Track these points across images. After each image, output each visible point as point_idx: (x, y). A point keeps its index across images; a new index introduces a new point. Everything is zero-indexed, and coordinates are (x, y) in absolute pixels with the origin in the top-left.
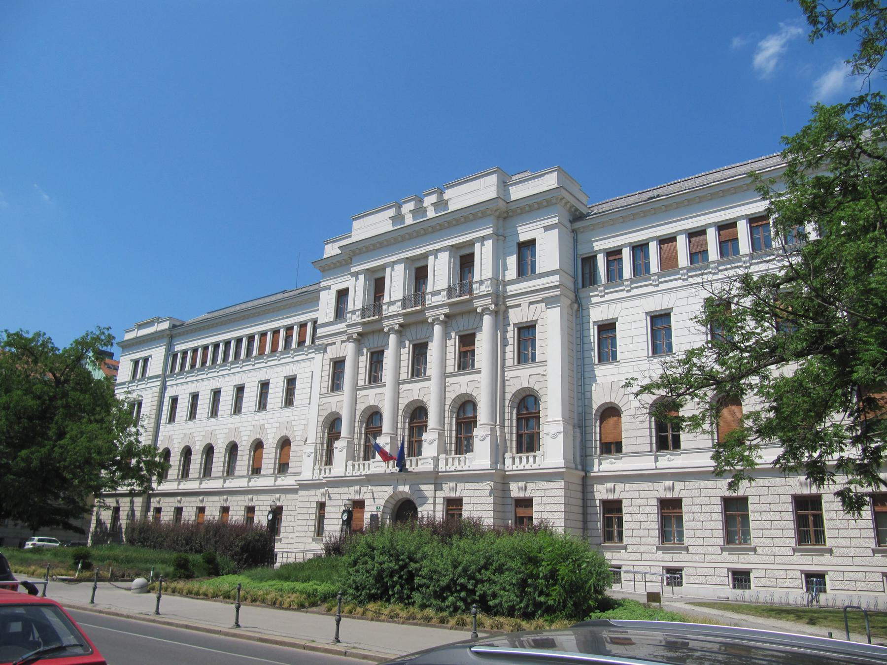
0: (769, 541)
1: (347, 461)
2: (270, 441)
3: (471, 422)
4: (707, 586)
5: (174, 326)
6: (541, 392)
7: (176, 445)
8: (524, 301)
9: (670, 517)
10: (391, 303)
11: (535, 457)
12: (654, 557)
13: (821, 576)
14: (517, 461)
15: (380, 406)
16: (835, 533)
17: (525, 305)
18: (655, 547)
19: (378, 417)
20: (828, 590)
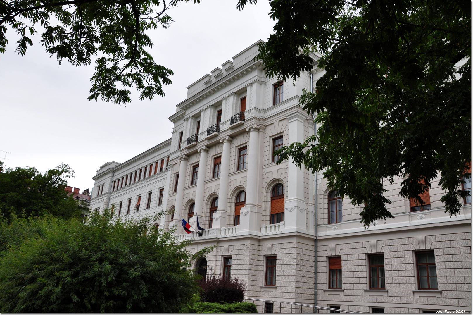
0: (453, 287)
3: (274, 197)
6: (284, 181)
8: (275, 120)
10: (225, 123)
11: (279, 225)
12: (411, 300)
14: (269, 229)
15: (244, 186)
17: (276, 123)
18: (411, 292)
19: (281, 187)
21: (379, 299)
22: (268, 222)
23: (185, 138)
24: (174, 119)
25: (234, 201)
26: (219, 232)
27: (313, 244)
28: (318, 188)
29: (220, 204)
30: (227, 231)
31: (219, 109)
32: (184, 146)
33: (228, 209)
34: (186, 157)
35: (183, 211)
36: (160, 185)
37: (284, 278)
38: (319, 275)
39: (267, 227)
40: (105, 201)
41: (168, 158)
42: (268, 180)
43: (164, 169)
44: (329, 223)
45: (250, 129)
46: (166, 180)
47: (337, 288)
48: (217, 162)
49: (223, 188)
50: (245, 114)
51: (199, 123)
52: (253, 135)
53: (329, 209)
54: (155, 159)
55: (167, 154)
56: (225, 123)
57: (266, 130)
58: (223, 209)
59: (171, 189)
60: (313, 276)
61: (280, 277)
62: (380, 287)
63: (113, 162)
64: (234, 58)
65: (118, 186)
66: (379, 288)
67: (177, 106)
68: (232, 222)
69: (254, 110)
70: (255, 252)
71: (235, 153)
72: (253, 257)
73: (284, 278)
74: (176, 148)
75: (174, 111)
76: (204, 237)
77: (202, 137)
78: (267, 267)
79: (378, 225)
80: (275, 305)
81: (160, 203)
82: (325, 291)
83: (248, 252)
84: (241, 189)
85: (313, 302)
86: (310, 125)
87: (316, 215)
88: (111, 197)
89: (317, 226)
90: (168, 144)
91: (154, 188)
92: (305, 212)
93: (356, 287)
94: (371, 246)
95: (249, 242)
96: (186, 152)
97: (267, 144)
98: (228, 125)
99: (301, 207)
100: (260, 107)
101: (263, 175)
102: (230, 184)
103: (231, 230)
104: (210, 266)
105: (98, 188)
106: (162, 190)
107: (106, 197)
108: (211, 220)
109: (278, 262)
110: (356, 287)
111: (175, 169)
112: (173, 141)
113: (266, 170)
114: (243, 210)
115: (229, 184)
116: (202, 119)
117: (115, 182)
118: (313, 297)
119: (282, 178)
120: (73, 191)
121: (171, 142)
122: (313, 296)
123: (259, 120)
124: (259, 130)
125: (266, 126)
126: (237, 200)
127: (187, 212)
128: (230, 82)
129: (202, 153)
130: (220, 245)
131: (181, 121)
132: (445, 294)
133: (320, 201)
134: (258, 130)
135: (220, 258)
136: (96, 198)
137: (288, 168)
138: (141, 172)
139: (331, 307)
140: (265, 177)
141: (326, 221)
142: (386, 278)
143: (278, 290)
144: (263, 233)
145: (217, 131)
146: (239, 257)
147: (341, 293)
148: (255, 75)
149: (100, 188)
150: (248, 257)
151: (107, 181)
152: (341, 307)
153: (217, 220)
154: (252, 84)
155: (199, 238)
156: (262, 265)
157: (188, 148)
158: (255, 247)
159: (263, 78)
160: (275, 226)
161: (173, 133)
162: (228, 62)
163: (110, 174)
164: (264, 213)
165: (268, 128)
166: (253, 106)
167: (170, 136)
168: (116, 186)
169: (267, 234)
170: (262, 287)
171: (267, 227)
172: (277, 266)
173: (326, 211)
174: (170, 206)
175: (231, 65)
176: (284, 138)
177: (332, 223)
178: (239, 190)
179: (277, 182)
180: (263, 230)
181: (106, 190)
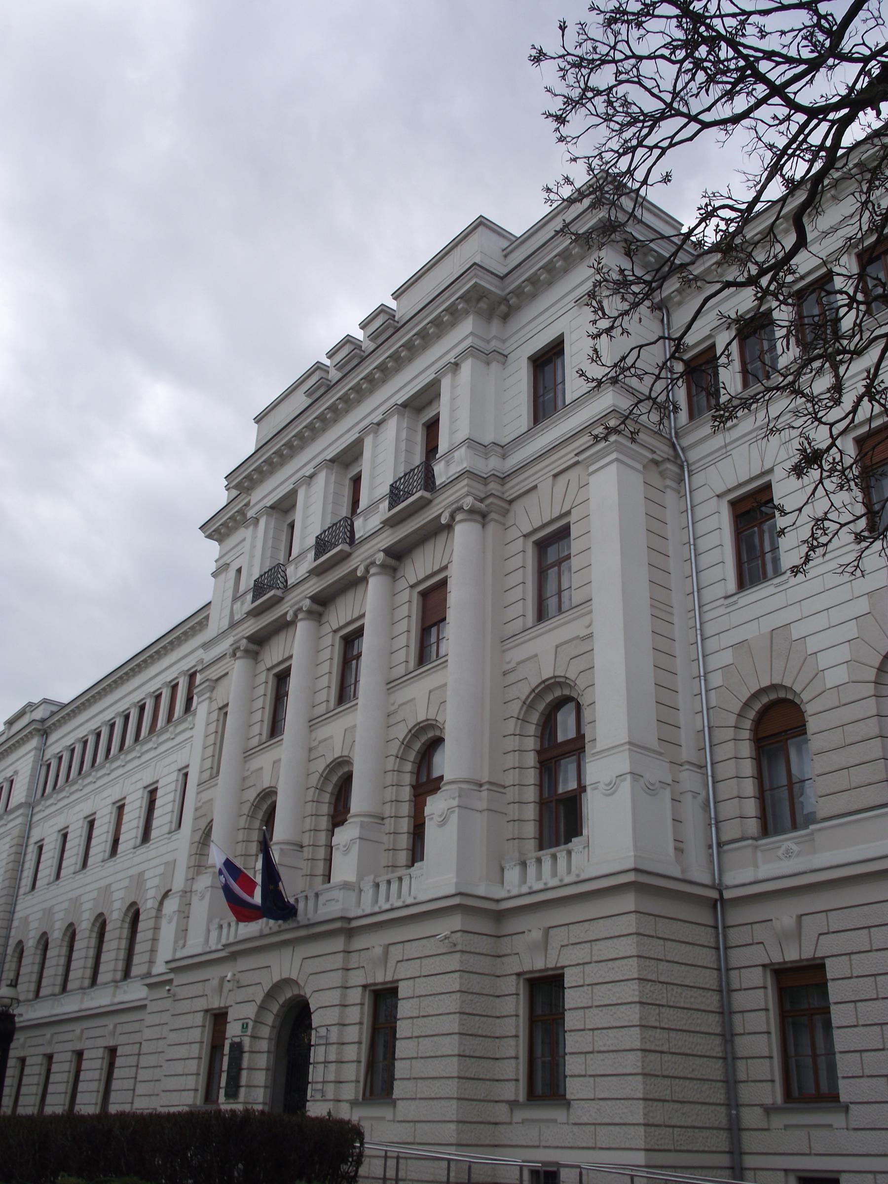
6: (581, 683)
8: (541, 474)
11: (569, 853)
14: (532, 870)
22: (531, 845)
24: (219, 528)
25: (407, 779)
26: (353, 896)
28: (713, 703)
29: (360, 800)
30: (383, 887)
31: (353, 472)
33: (388, 810)
34: (252, 647)
38: (745, 1045)
39: (524, 864)
40: (16, 832)
42: (524, 691)
44: (766, 831)
45: (452, 517)
49: (363, 735)
52: (464, 533)
53: (759, 777)
56: (373, 506)
60: (717, 1051)
61: (580, 1059)
63: (45, 701)
64: (396, 296)
68: (403, 857)
69: (463, 450)
70: (484, 964)
73: (597, 1064)
75: (218, 496)
78: (533, 1021)
82: (769, 1110)
83: (454, 962)
84: (431, 734)
86: (669, 482)
88: (35, 819)
92: (667, 794)
95: (456, 922)
97: (517, 561)
100: (487, 439)
101: (505, 674)
102: (392, 720)
103: (394, 886)
104: (323, 1031)
107: (19, 820)
109: (571, 998)
113: (516, 655)
114: (435, 806)
117: (49, 766)
118: (720, 1141)
119: (571, 675)
122: (724, 1135)
123: (485, 480)
124: (484, 516)
125: (511, 502)
126: (418, 773)
128: (385, 372)
130: (359, 943)
134: (481, 516)
135: (355, 996)
137: (590, 636)
140: (511, 678)
141: (753, 826)
143: (581, 1112)
144: (513, 885)
146: (422, 986)
147: (837, 1120)
150: (454, 983)
156: (513, 1008)
158: (484, 945)
162: (382, 310)
163: (34, 742)
164: (513, 811)
166: (462, 434)
170: (513, 1104)
172: (568, 1016)
173: (749, 787)
176: (574, 531)
177: (777, 833)
178: (423, 739)
180: (512, 875)
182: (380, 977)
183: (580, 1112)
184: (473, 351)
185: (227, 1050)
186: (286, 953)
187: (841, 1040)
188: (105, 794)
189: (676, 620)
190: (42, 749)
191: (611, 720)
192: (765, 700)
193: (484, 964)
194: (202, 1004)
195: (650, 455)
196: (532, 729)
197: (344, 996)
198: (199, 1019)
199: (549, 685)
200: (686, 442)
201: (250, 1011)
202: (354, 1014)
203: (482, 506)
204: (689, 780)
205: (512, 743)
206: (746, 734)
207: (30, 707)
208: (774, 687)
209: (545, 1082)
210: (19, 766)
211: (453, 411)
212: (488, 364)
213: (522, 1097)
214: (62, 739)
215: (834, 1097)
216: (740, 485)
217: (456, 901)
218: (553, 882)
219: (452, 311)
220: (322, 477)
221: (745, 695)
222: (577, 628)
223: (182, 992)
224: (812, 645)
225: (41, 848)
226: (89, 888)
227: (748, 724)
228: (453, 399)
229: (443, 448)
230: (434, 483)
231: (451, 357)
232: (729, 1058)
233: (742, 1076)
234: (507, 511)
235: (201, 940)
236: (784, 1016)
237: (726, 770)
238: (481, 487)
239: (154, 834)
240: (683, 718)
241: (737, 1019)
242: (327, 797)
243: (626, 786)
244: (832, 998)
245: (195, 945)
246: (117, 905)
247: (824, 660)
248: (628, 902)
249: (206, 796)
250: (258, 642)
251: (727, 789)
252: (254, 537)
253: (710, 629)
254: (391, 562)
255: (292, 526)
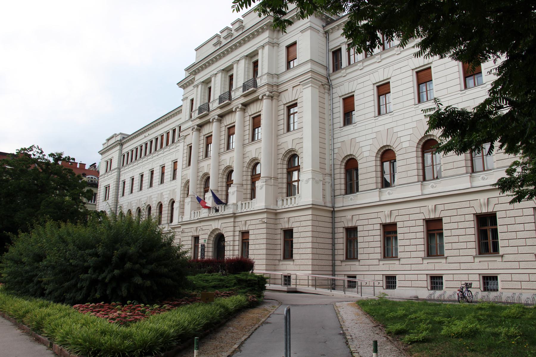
1: (191, 211)
2: (166, 203)
4: (412, 288)
5: (124, 138)
7: (166, 199)
9: (434, 234)
10: (237, 89)
11: (295, 198)
12: (376, 268)
13: (494, 278)
16: (505, 243)
18: (421, 259)
20: (444, 288)
21: (437, 266)
22: (285, 195)
23: (196, 106)
24: (184, 85)
27: (330, 215)
30: (244, 205)
31: (230, 74)
32: (196, 115)
33: (244, 182)
35: (198, 186)
36: (173, 158)
37: (301, 251)
41: (180, 127)
42: (283, 151)
43: (176, 140)
44: (346, 193)
46: (177, 152)
47: (392, 257)
48: (231, 132)
50: (257, 81)
51: (210, 88)
54: (166, 129)
55: (178, 123)
56: (237, 89)
57: (280, 97)
58: (238, 183)
59: (185, 162)
62: (492, 252)
63: (121, 134)
65: (136, 156)
66: (491, 253)
67: (187, 70)
68: (249, 196)
69: (266, 76)
70: (272, 226)
71: (249, 123)
72: (270, 231)
73: (301, 251)
74: (188, 117)
75: (182, 75)
76: (220, 213)
77: (214, 105)
78: (285, 241)
79: (431, 188)
80: (293, 277)
81: (174, 178)
82: (342, 261)
83: (264, 226)
84: (256, 161)
85: (331, 273)
86: (326, 91)
87: (333, 186)
88: (121, 173)
89: (334, 196)
90: (179, 111)
91: (156, 166)
92: (321, 183)
93: (371, 256)
94: (386, 216)
95: (265, 216)
96: (199, 122)
98: (240, 92)
99: (316, 178)
100: (274, 72)
101: (278, 146)
104: (228, 242)
105: (105, 164)
106: (175, 163)
108: (227, 195)
110: (371, 256)
111: (189, 140)
112: (183, 108)
115: (219, 164)
116: (212, 84)
117: (124, 155)
119: (297, 149)
120: (78, 166)
121: (181, 110)
123: (272, 86)
124: (272, 97)
125: (280, 93)
127: (203, 186)
128: (241, 44)
129: (264, 101)
130: (237, 220)
131: (191, 88)
132: (506, 258)
133: (337, 171)
134: (271, 97)
135: (237, 233)
136: (104, 174)
137: (302, 138)
138: (128, 155)
139: (348, 277)
141: (343, 192)
142: (444, 244)
145: (254, 87)
148: (265, 36)
149: (109, 163)
151: (115, 154)
152: (357, 276)
153: (233, 194)
154: (263, 47)
155: (216, 214)
156: (280, 238)
157: (200, 118)
158: (272, 221)
159: (275, 40)
160: (291, 199)
161: (183, 100)
163: (118, 148)
165: (283, 95)
167: (181, 103)
168: (127, 159)
169: (283, 207)
171: (283, 200)
174: (185, 181)
175: (241, 24)
179: (293, 153)
180: (280, 203)
181: (115, 165)
182: (244, 229)
183: (296, 262)
184: (269, 43)
185: (200, 246)
186: (217, 222)
187: (360, 245)
188: (146, 167)
189: (326, 133)
190: (121, 150)
191: (306, 162)
192: (348, 158)
193: (272, 226)
194: (191, 234)
195: (321, 84)
196: (285, 162)
197: (234, 234)
198: (190, 238)
199: (290, 151)
200: (332, 78)
201: (207, 237)
202: (237, 238)
203: (271, 94)
204: (328, 179)
205: (280, 166)
206: (343, 167)
207: (115, 135)
208: (351, 155)
209: (288, 254)
210: (113, 155)
211: (262, 58)
212: (273, 47)
213: (282, 258)
214: (128, 147)
215: (357, 259)
216: (346, 95)
217: (265, 210)
218: (291, 206)
219: (262, 28)
220: (219, 75)
221: (343, 157)
222: (298, 135)
223: (186, 230)
224: (361, 144)
225: (124, 183)
226: (143, 197)
227: (344, 164)
228: (262, 65)
229: (259, 74)
230: (257, 84)
231: (262, 44)
232: (333, 249)
233: (336, 253)
234: (279, 96)
235: (189, 216)
236: (347, 239)
237: (337, 176)
238: (271, 88)
239: (125, 194)
240: (327, 162)
241: (336, 240)
242: (225, 177)
243: (311, 181)
244: (358, 236)
245: (186, 218)
246: (154, 202)
247: (364, 149)
248: (310, 212)
249: (185, 173)
250: (200, 126)
251: (337, 182)
252: (197, 91)
253: (335, 136)
254: (244, 107)
255: (210, 88)
